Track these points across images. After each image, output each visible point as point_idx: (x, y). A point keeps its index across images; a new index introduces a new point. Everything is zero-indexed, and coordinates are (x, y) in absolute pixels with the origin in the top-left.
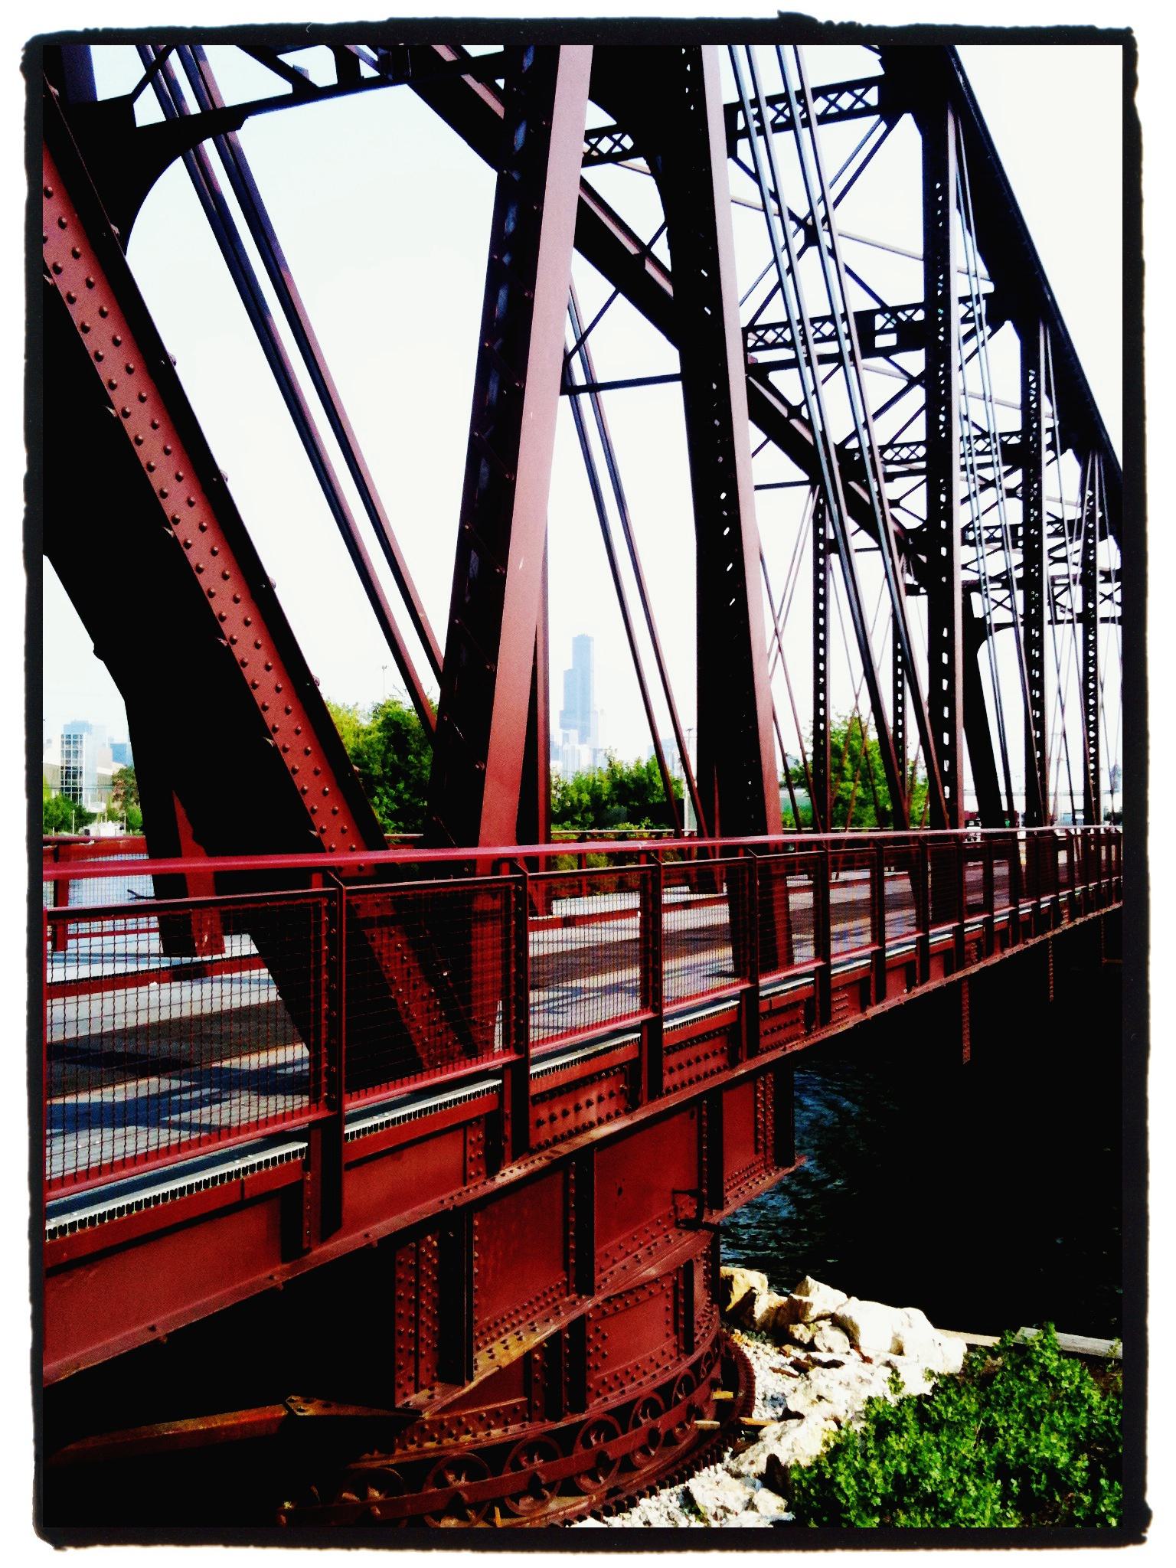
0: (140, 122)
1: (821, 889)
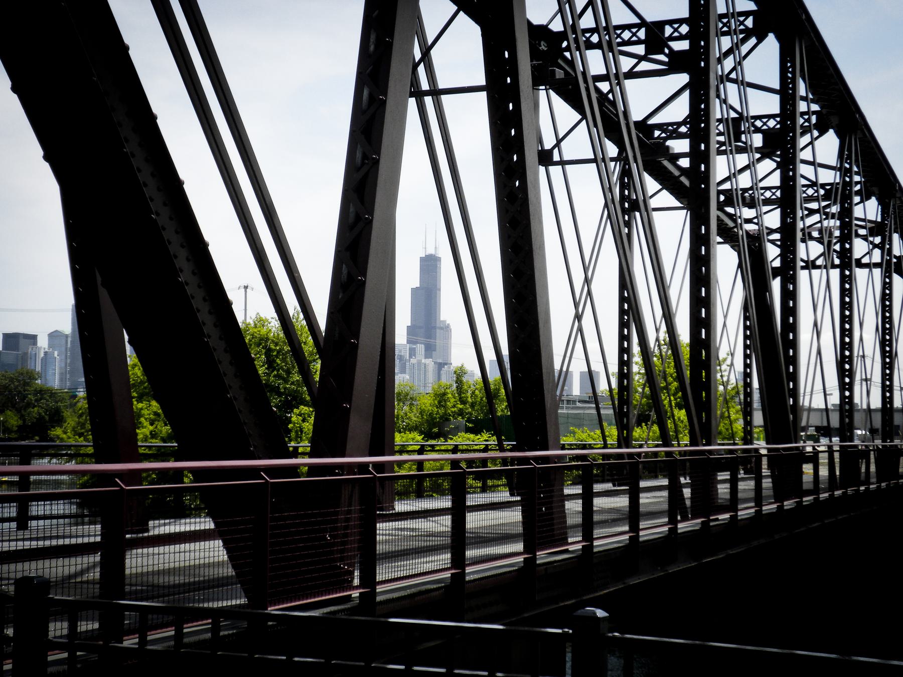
0: (688, 166)
1: (587, 497)
